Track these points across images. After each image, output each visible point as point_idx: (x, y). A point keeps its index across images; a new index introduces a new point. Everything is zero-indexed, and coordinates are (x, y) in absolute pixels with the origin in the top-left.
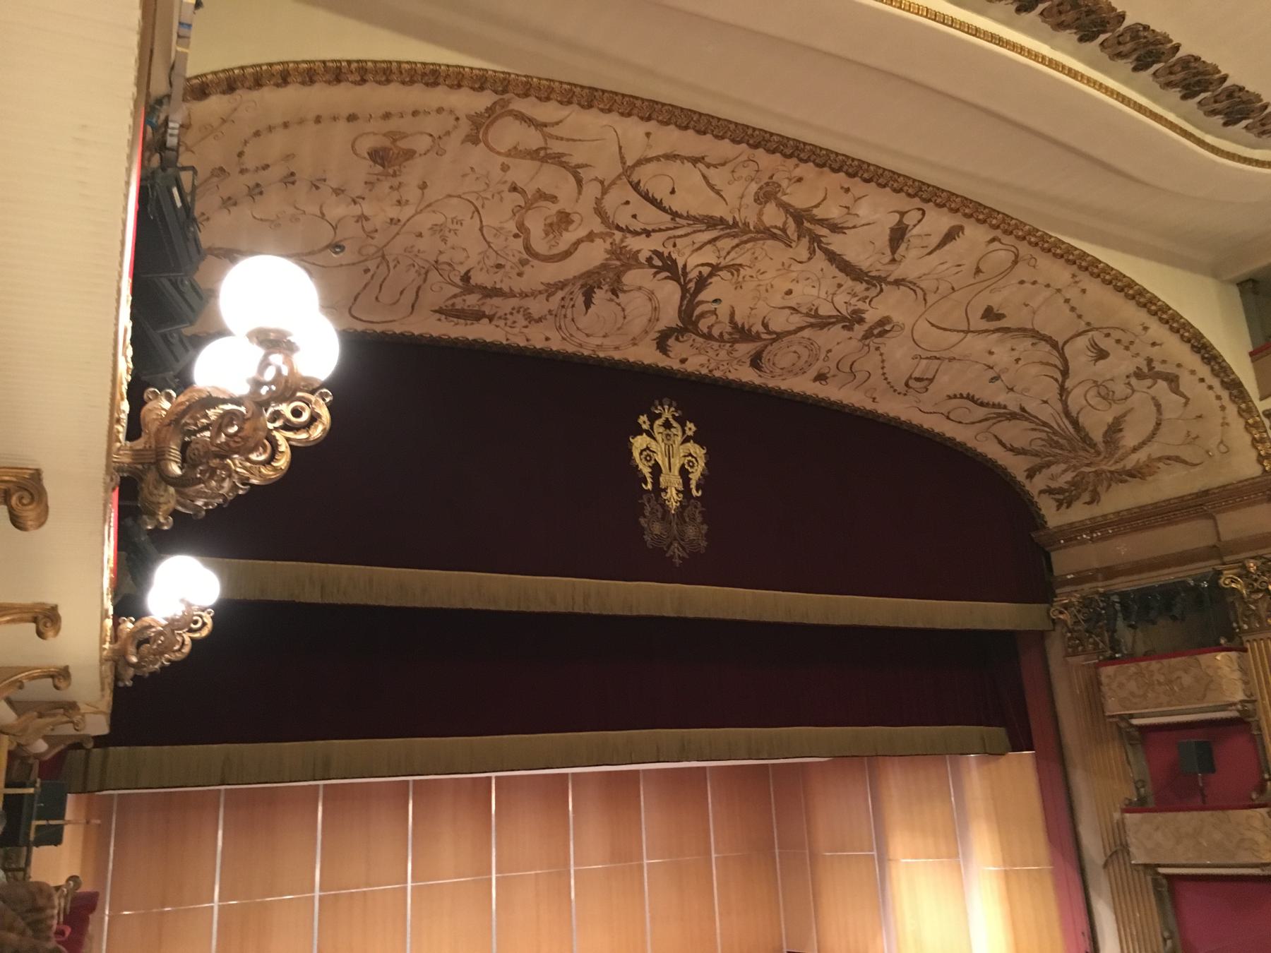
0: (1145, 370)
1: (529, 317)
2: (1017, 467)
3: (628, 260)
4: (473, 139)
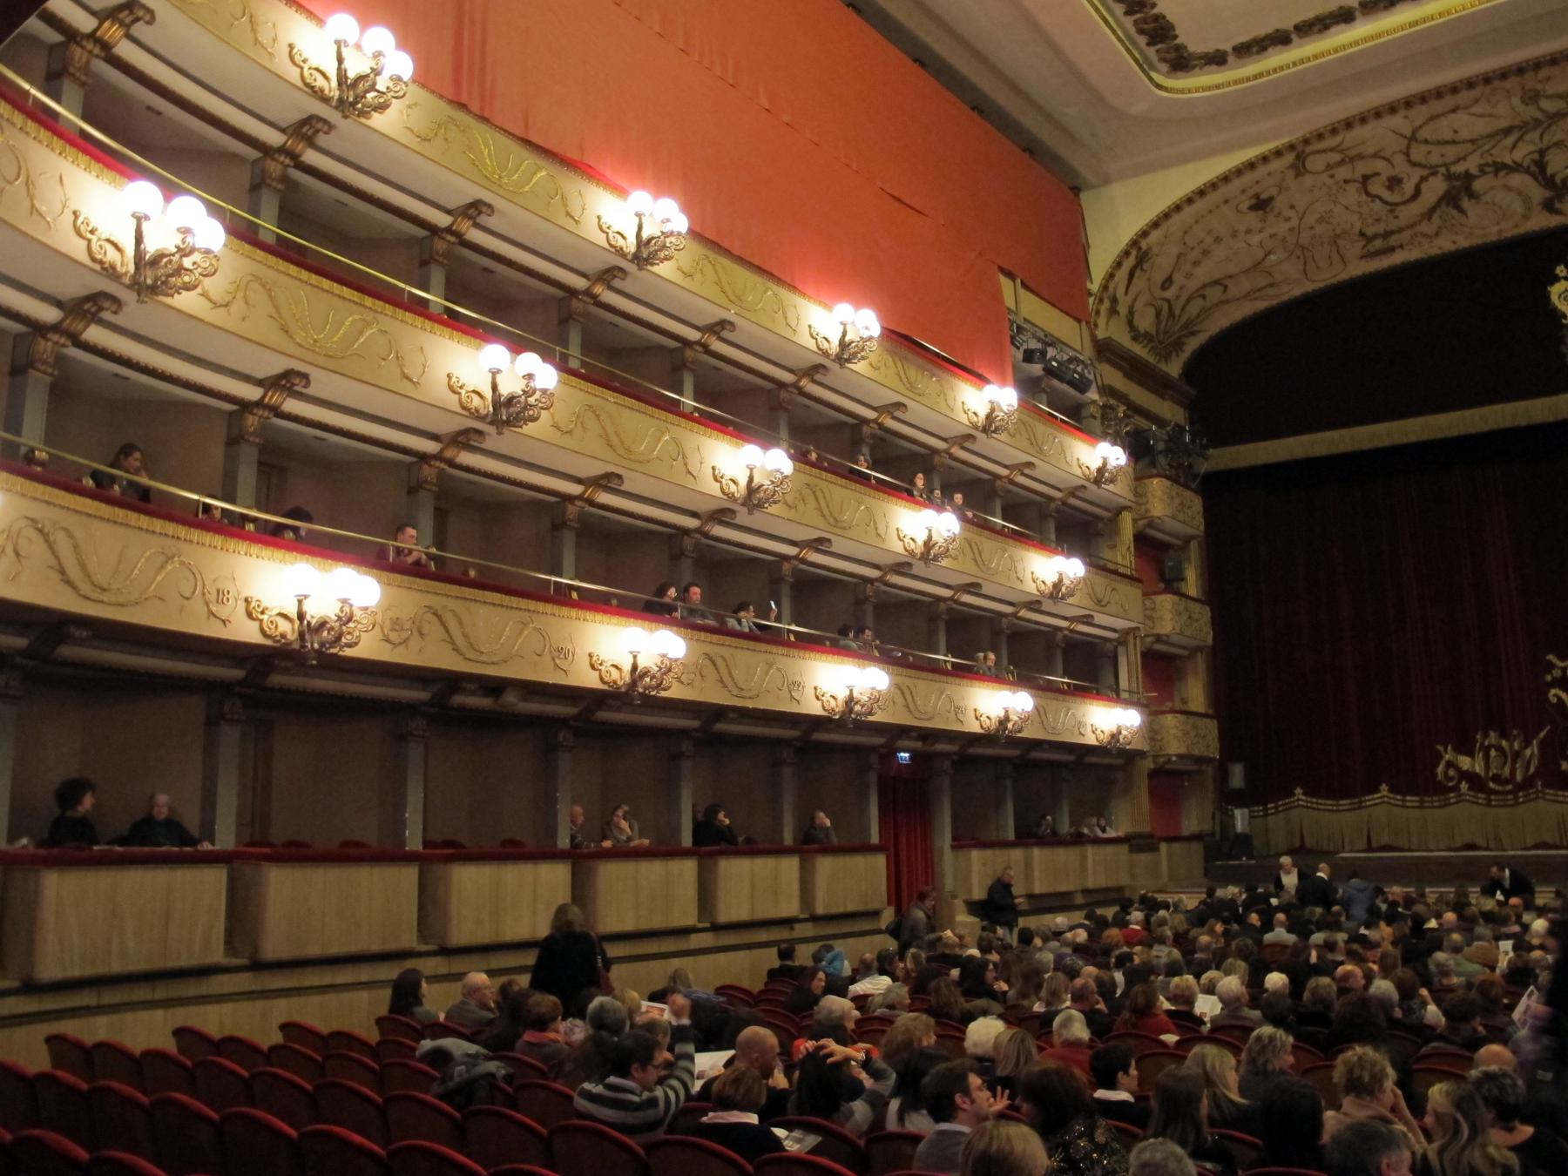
1: (1425, 236)
3: (1468, 177)
4: (1298, 175)
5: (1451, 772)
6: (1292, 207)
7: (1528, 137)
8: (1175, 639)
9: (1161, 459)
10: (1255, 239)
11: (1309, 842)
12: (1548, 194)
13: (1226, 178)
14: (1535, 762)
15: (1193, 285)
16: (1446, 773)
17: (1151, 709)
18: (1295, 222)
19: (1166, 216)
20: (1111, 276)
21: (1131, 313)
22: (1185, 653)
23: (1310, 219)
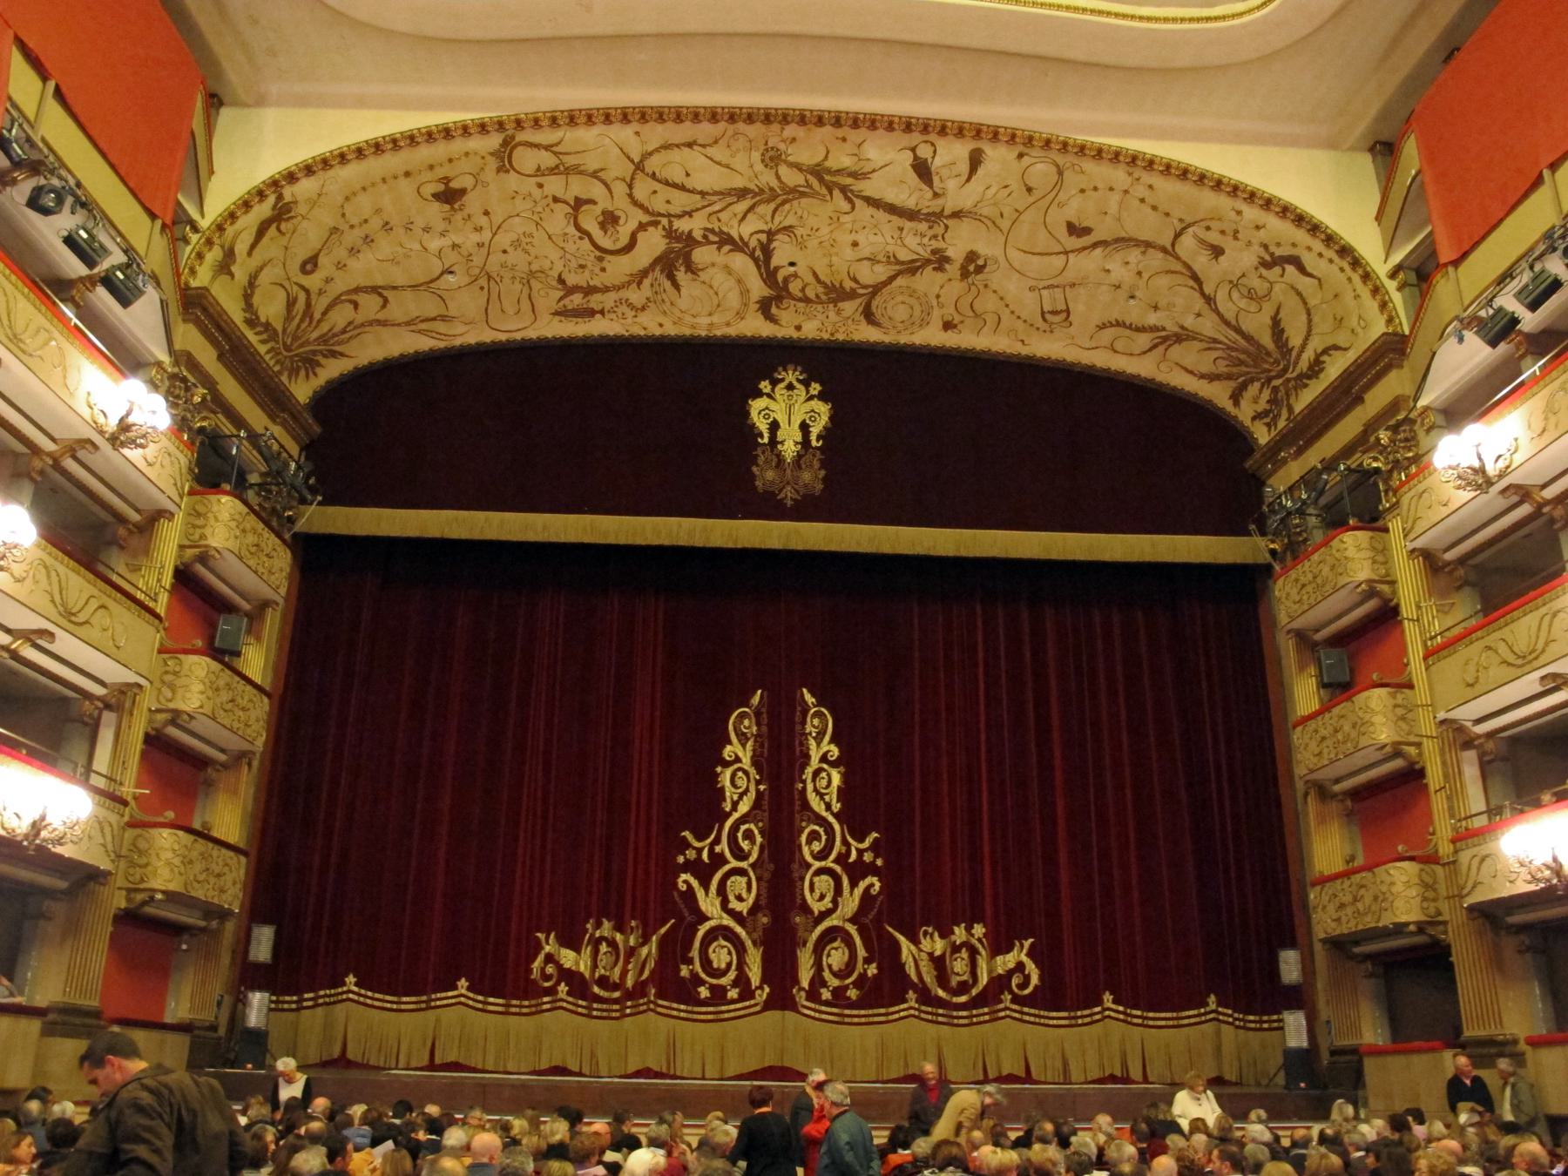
0: (1268, 258)
1: (631, 306)
2: (1217, 394)
3: (689, 241)
4: (500, 169)
5: (550, 969)
6: (486, 213)
7: (761, 209)
8: (202, 725)
9: (251, 495)
10: (435, 244)
11: (350, 1055)
12: (767, 292)
13: (412, 139)
14: (651, 964)
15: (340, 286)
16: (543, 970)
17: (129, 819)
18: (486, 236)
19: (326, 163)
20: (232, 216)
21: (252, 283)
22: (222, 757)
23: (504, 240)
